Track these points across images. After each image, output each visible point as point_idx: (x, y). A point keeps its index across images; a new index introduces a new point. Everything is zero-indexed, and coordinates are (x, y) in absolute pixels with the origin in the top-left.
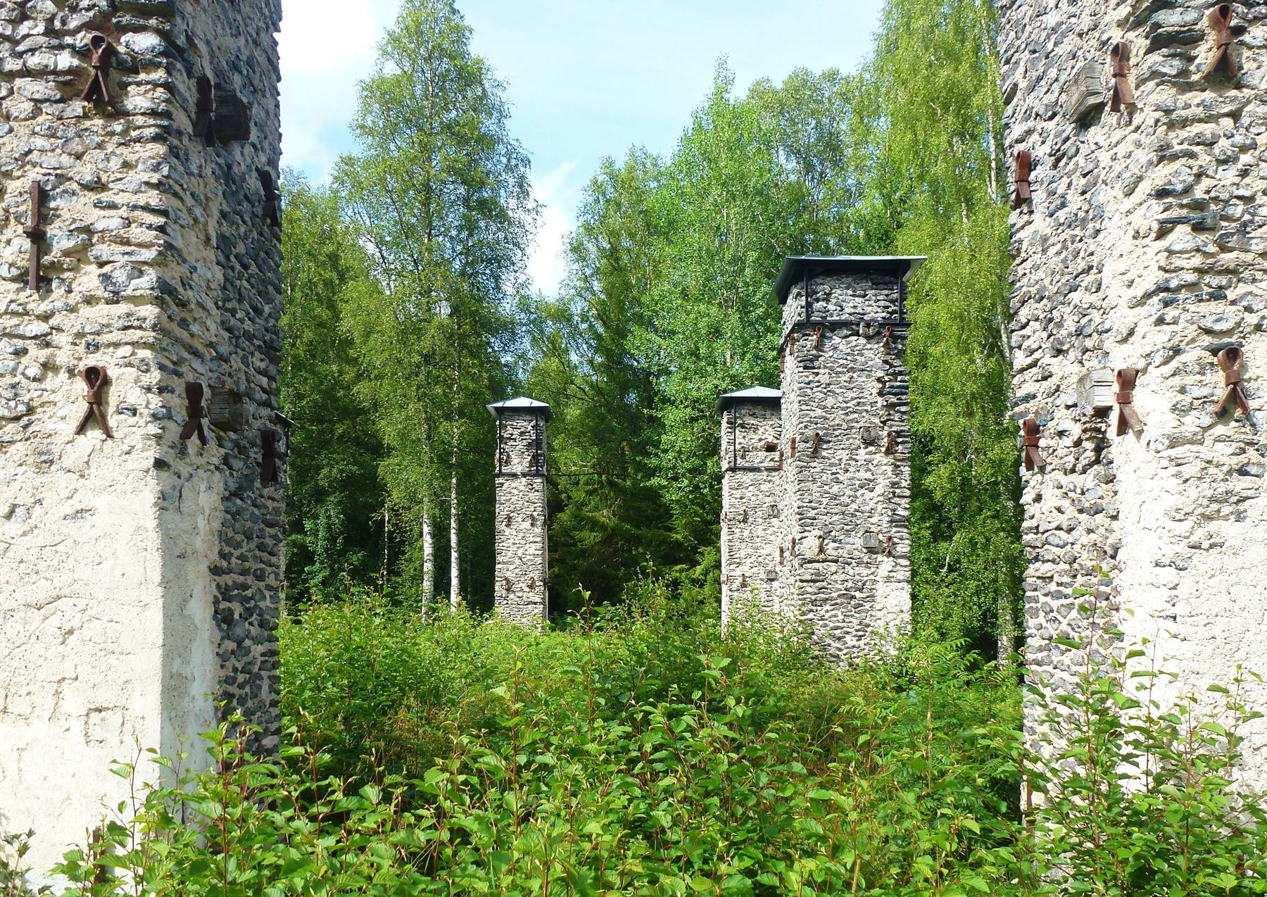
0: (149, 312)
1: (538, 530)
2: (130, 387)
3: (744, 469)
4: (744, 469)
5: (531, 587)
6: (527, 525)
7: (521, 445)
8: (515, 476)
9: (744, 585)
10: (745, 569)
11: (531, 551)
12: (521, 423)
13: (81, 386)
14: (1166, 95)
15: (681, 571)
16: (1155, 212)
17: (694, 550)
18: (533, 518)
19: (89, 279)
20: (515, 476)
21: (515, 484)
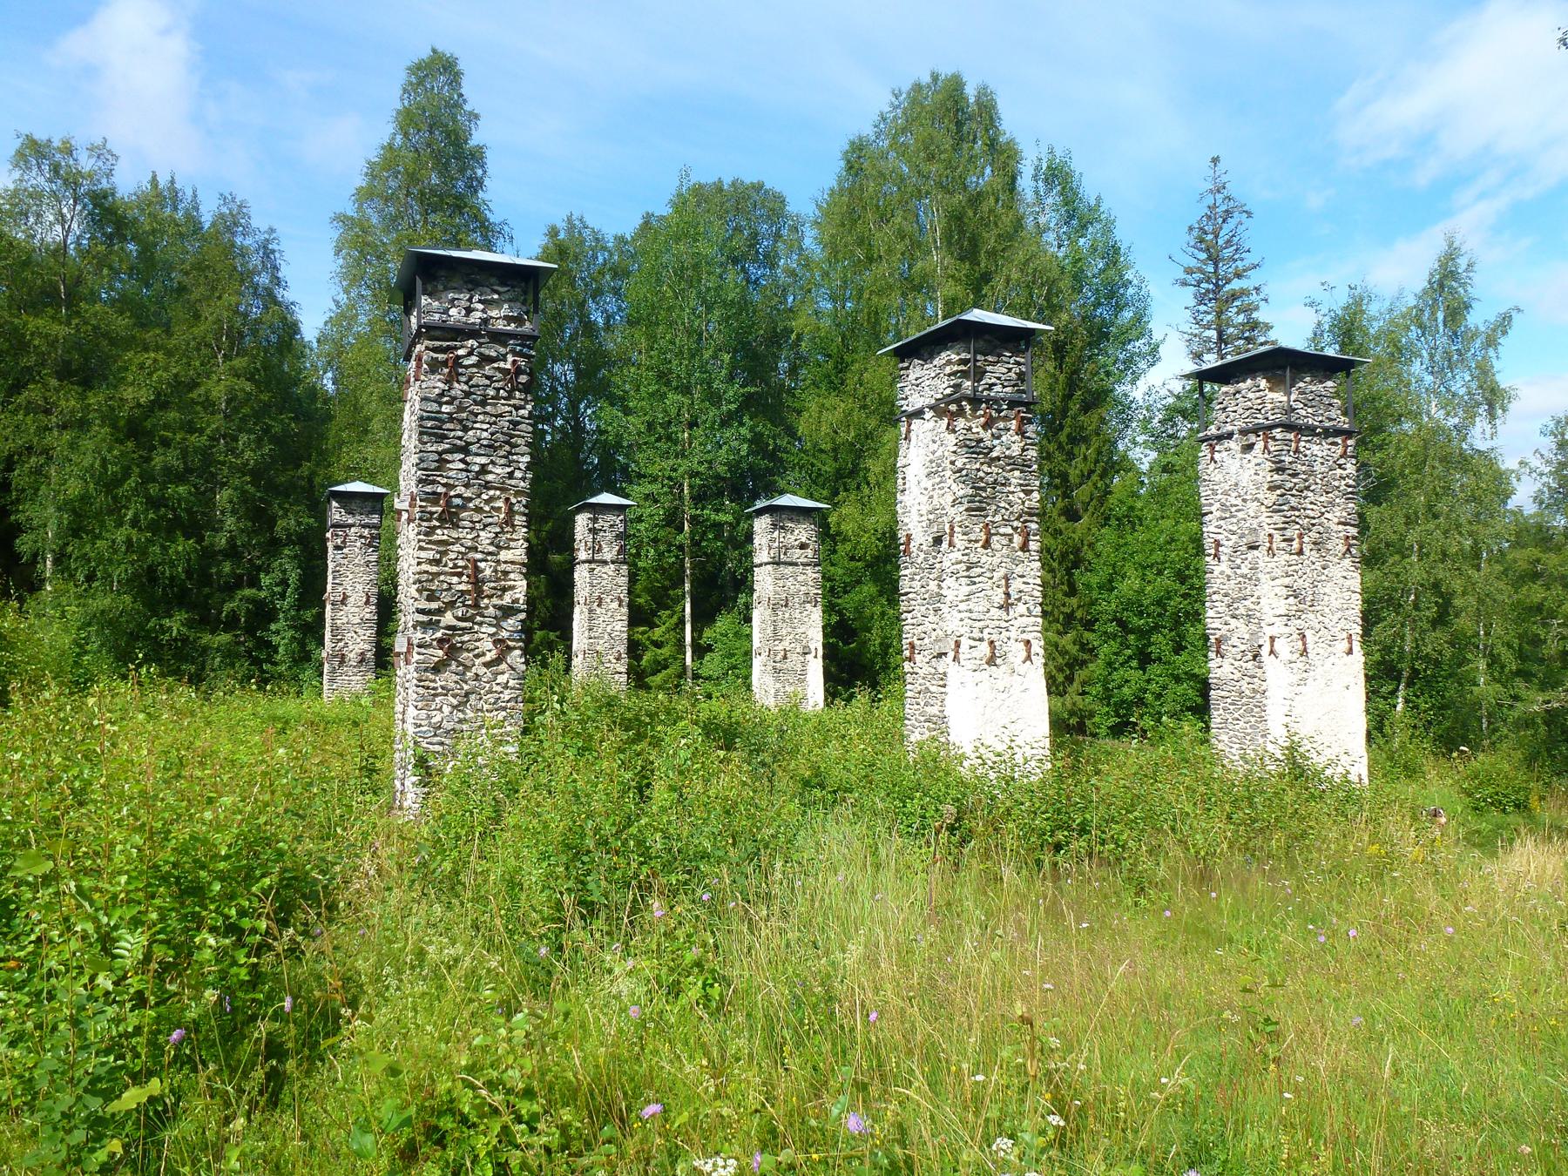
0: (1040, 620)
1: (625, 610)
2: (1038, 647)
3: (785, 563)
4: (785, 563)
5: (618, 659)
6: (615, 605)
7: (609, 536)
8: (605, 563)
9: (785, 657)
10: (786, 644)
11: (618, 628)
12: (610, 517)
13: (1022, 646)
14: (1287, 557)
15: (643, 633)
16: (1285, 592)
17: (654, 613)
18: (621, 601)
19: (1021, 608)
20: (605, 563)
21: (606, 569)
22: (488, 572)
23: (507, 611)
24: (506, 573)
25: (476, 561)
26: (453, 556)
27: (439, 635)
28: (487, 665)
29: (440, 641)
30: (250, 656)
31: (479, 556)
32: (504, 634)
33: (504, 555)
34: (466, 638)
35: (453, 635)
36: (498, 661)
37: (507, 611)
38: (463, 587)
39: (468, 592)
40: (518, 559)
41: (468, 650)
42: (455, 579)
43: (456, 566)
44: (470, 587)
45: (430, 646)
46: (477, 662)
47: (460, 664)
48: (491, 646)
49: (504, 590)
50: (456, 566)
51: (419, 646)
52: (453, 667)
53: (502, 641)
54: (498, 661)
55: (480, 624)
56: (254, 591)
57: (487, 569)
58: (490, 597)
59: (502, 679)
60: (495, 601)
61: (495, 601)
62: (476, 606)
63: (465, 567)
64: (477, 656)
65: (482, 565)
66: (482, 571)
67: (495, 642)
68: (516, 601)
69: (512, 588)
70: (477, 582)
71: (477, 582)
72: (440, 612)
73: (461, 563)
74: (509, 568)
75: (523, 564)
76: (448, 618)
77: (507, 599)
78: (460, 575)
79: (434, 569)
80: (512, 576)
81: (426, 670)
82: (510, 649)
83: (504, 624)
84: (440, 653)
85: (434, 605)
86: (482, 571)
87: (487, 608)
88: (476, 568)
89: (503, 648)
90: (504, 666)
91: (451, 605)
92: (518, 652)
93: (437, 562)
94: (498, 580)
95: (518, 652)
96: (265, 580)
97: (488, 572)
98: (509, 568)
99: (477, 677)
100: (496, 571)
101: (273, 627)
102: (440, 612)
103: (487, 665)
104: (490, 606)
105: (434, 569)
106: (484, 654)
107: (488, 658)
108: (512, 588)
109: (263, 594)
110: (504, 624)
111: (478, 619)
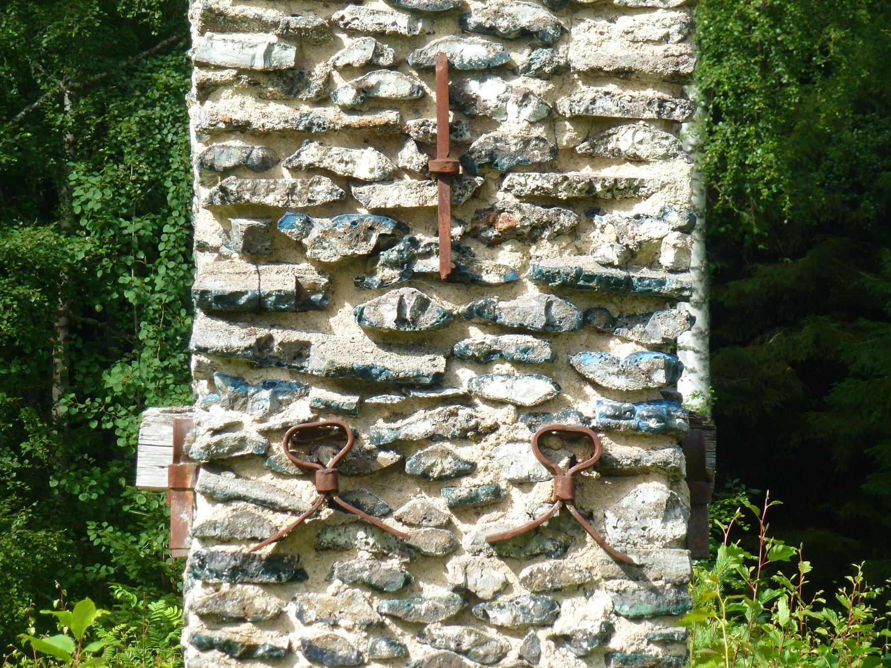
22: (514, 124)
23: (608, 303)
24: (597, 126)
25: (458, 73)
26: (355, 51)
27: (299, 411)
28: (511, 548)
29: (304, 438)
30: (41, 491)
31: (473, 50)
32: (592, 407)
33: (591, 42)
34: (418, 425)
35: (360, 412)
36: (563, 528)
37: (608, 303)
38: (403, 195)
39: (425, 215)
40: (652, 58)
41: (431, 482)
42: (366, 162)
43: (368, 100)
44: (431, 194)
45: (260, 459)
46: (474, 532)
47: (390, 544)
48: (524, 459)
49: (590, 203)
50: (368, 100)
51: (217, 463)
52: (361, 559)
53: (577, 438)
54: (563, 528)
55: (484, 360)
56: (46, 234)
57: (510, 110)
58: (526, 237)
59: (580, 616)
60: (549, 256)
61: (549, 256)
62: (462, 277)
63: (415, 103)
64: (470, 508)
65: (487, 92)
66: (488, 121)
67: (544, 444)
68: (639, 254)
69: (628, 192)
70: (465, 172)
71: (465, 172)
72: (303, 305)
73: (392, 85)
74: (608, 100)
75: (676, 81)
76: (342, 339)
77: (602, 247)
78: (388, 139)
79: (275, 114)
80: (623, 139)
81: (238, 572)
82: (615, 474)
83: (590, 363)
84: (305, 493)
85: (277, 279)
86: (488, 121)
87: (510, 285)
88: (461, 103)
89: (586, 470)
90: (586, 558)
91: (353, 273)
92: (653, 492)
93: (288, 82)
94: (558, 158)
95: (653, 492)
96: (88, 191)
97: (514, 124)
98: (608, 100)
99: (468, 605)
100: (550, 118)
101: (115, 379)
102: (303, 305)
103: (511, 548)
104: (522, 279)
105: (275, 114)
106: (497, 499)
107: (522, 511)
108: (628, 192)
109: (80, 248)
110: (590, 363)
111: (477, 337)
